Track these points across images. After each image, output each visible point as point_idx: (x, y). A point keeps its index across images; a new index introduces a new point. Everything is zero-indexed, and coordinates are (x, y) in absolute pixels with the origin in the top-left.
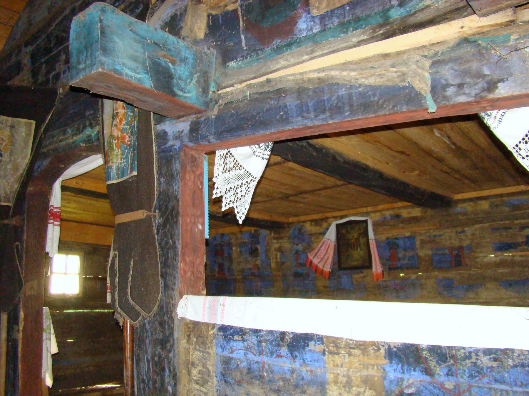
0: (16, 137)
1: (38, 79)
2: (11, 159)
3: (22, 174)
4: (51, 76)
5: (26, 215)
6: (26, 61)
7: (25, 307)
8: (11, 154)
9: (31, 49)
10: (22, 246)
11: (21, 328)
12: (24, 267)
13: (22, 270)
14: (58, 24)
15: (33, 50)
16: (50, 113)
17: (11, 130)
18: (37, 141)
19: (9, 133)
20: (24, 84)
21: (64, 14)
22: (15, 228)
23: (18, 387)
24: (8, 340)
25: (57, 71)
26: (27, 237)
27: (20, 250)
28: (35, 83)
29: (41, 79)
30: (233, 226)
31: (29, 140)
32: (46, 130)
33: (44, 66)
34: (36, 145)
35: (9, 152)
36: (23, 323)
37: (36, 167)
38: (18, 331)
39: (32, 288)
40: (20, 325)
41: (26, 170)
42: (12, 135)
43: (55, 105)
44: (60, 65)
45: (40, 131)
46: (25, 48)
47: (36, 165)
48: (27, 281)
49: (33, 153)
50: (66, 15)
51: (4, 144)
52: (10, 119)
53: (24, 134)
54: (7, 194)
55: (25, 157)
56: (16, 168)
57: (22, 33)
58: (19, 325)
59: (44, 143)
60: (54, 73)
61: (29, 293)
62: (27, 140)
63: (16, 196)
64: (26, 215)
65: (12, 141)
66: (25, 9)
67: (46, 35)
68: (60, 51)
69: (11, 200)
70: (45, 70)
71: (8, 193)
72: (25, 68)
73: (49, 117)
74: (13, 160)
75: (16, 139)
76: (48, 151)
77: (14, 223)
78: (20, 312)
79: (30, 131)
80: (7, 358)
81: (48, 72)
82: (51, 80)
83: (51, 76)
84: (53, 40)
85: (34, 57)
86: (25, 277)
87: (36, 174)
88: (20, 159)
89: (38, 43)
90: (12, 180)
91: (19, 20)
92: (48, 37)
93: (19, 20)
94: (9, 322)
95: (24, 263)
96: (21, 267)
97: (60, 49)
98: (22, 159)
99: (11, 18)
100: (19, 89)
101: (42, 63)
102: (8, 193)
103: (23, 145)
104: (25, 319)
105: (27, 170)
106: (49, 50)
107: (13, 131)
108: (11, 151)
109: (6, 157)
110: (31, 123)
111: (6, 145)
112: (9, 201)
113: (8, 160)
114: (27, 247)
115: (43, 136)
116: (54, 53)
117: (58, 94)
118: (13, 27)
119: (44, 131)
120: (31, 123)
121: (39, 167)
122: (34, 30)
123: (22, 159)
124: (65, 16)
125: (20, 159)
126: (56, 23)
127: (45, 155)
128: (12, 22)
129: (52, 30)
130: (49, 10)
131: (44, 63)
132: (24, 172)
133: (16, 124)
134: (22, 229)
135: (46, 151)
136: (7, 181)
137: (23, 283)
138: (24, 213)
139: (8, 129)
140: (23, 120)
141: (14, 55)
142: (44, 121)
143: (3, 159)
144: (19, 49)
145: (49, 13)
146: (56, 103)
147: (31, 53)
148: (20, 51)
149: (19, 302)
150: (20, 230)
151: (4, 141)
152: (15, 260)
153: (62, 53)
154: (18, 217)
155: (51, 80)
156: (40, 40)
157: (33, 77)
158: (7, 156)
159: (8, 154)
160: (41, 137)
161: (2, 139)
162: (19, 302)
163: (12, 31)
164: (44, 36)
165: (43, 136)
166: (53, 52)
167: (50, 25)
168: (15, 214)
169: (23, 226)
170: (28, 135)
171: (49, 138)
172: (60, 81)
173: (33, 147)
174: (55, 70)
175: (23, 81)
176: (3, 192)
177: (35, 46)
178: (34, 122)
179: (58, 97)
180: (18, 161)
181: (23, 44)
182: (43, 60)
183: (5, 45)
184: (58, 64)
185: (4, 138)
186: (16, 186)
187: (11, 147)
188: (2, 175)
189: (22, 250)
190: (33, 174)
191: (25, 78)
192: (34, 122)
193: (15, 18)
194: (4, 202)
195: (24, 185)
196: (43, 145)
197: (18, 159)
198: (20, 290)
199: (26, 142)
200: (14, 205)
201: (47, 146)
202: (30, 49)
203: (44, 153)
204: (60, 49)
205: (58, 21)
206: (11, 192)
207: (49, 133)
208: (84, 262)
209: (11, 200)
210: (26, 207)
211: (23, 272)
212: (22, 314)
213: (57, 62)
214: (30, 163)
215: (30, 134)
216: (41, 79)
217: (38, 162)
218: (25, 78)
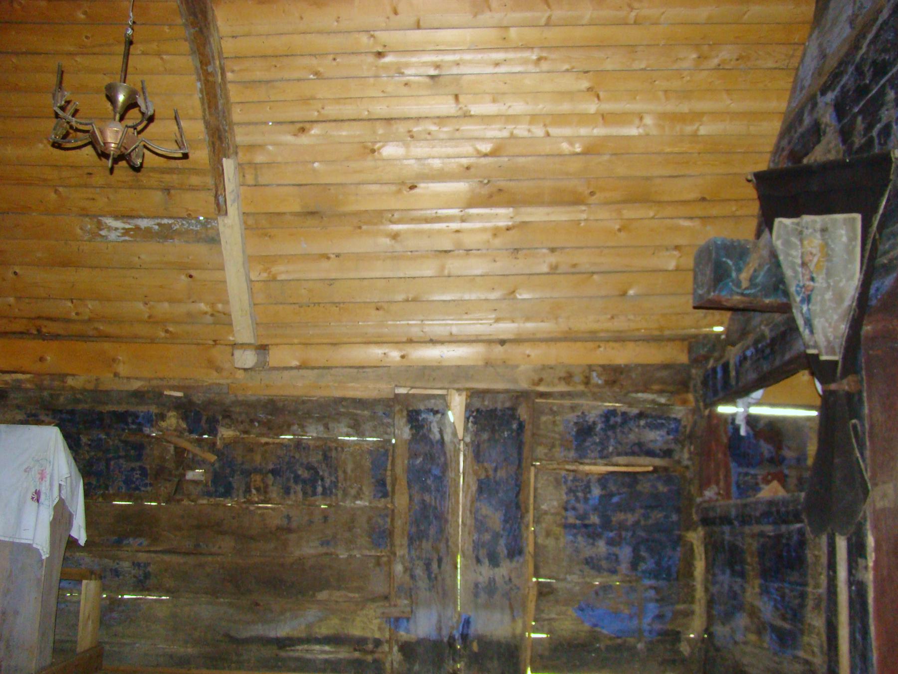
0: (833, 246)
1: (853, 143)
2: (828, 284)
3: (850, 306)
4: (874, 133)
5: (864, 373)
6: (828, 118)
7: (875, 528)
8: (829, 275)
9: (833, 97)
10: (863, 425)
11: (871, 564)
12: (868, 461)
13: (866, 465)
14: (873, 42)
15: (836, 97)
16: (882, 195)
17: (822, 236)
18: (868, 247)
19: (820, 242)
20: (832, 157)
21: (880, 21)
22: (849, 396)
23: (872, 665)
24: (850, 583)
25: (884, 121)
26: (870, 410)
27: (860, 433)
28: (849, 151)
29: (858, 141)
30: (778, 150)
31: (854, 247)
32: (882, 226)
33: (859, 119)
34: (867, 254)
35: (824, 271)
36: (873, 555)
37: (872, 291)
38: (866, 568)
39: (884, 496)
40: (868, 558)
41: (856, 298)
42: (826, 245)
43: (891, 180)
44: (887, 110)
45: (870, 230)
46: (823, 98)
47: (872, 287)
48: (875, 485)
49: (864, 268)
50: (884, 21)
51: (815, 260)
52: (818, 218)
53: (844, 239)
54: (829, 342)
55: (851, 278)
56: (839, 297)
57: (813, 74)
58: (866, 558)
59: (881, 248)
60: (879, 126)
61: (879, 505)
62: (851, 247)
63: (844, 343)
64: (864, 373)
65: (827, 251)
66: (810, 36)
67: (853, 67)
68: (883, 86)
69: (837, 350)
70: (863, 126)
71: (831, 339)
72: (828, 129)
73: (884, 203)
74: (832, 284)
75: (833, 250)
76: (891, 261)
77: (846, 388)
78: (866, 536)
79: (854, 230)
80: (850, 613)
81: (869, 127)
82: (876, 141)
83: (874, 133)
84: (868, 71)
85: (840, 109)
86: (871, 478)
87: (874, 302)
88: (844, 280)
89: (842, 83)
90: (836, 317)
91: (804, 55)
92: (859, 71)
93: (804, 55)
94: (850, 553)
95: (867, 453)
96: (864, 461)
97: (882, 82)
98: (848, 280)
99: (792, 56)
100: (826, 167)
101: (855, 117)
102: (831, 339)
103: (845, 256)
104: (878, 548)
105: (858, 298)
106: (866, 89)
107: (827, 237)
108: (828, 269)
109: (820, 281)
110: (854, 219)
111: (818, 261)
112: (834, 353)
113: (825, 285)
114: (872, 426)
115: (877, 237)
116: (874, 92)
117: (893, 160)
118: (797, 69)
119: (878, 228)
120: (854, 219)
121: (877, 290)
122: (832, 63)
123: (848, 280)
124: (881, 25)
125: (844, 280)
126: (867, 41)
127: (887, 269)
128: (795, 62)
129: (863, 54)
130: (852, 22)
131: (859, 112)
132: (853, 302)
133: (829, 226)
134: (860, 400)
135: (886, 261)
136: (827, 320)
137: (870, 487)
138: (862, 369)
139: (818, 235)
140: (839, 217)
141: (806, 114)
142: (875, 210)
143: (816, 285)
144: (812, 101)
145: (852, 28)
146: (892, 177)
147: (833, 103)
148: (815, 105)
149: (865, 518)
150: (856, 399)
151: (815, 255)
152: (853, 449)
153: (888, 89)
154: (851, 378)
155: (876, 141)
156: (845, 79)
157: (844, 142)
158: (823, 279)
159: (824, 276)
160: (874, 240)
161: (811, 253)
162: (865, 520)
163: (796, 75)
164: (851, 69)
165: (877, 237)
166: (872, 90)
167: (856, 47)
168: (845, 374)
169: (860, 392)
170: (852, 239)
171: (889, 239)
172: (892, 137)
173: (862, 256)
174: (879, 121)
175: (829, 151)
176: (824, 339)
177: (838, 89)
178: (858, 217)
179: (893, 165)
180: (841, 284)
181: (819, 93)
182: (856, 110)
183: (789, 103)
184: (885, 108)
185: (814, 251)
186: (843, 328)
187: (826, 264)
188: (818, 311)
189: (864, 433)
190: (869, 304)
191: (832, 145)
192: (858, 217)
193: (799, 53)
194: (827, 354)
195: (855, 325)
196: (879, 253)
197: (841, 281)
198: (865, 499)
199: (850, 252)
200: (843, 358)
201: (885, 253)
202: (830, 96)
203: (884, 266)
204: (882, 82)
205: (870, 37)
206: (835, 338)
207: (887, 231)
208: (614, 331)
209: (837, 350)
210: (863, 360)
211: (868, 469)
212: (870, 541)
213: (882, 105)
214: (862, 285)
215: (855, 239)
216: (858, 141)
217: (874, 282)
218: (832, 145)
